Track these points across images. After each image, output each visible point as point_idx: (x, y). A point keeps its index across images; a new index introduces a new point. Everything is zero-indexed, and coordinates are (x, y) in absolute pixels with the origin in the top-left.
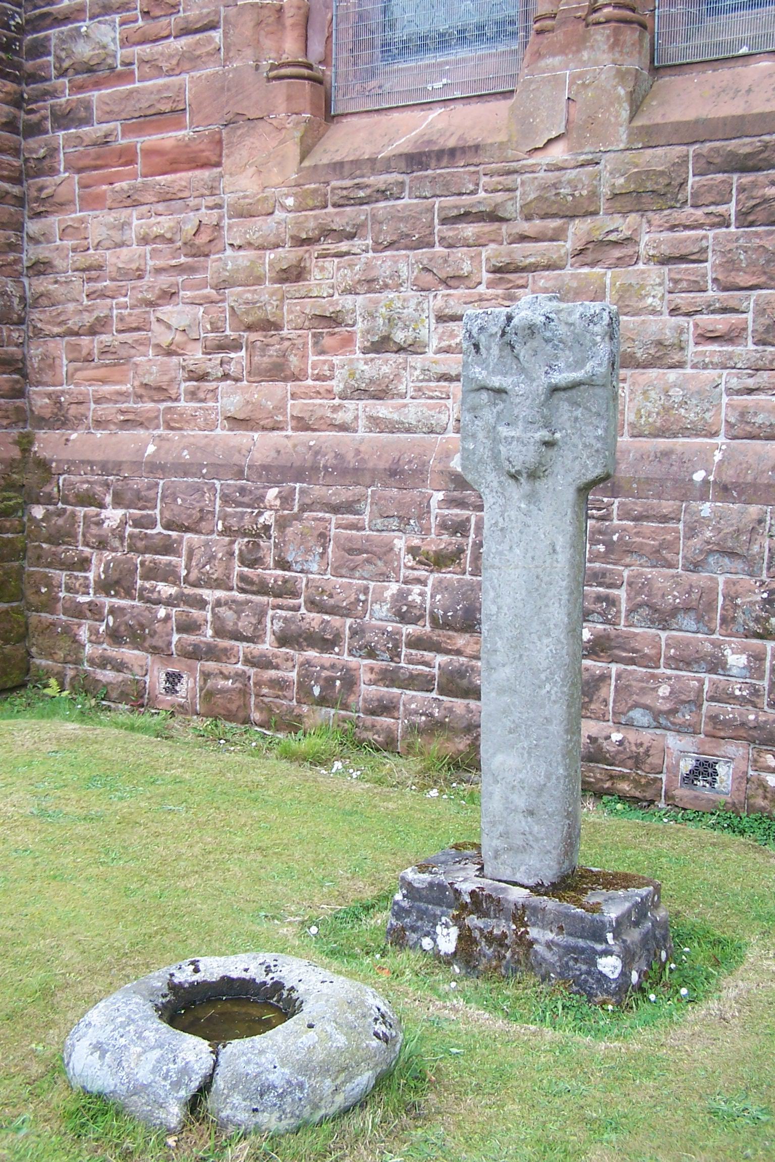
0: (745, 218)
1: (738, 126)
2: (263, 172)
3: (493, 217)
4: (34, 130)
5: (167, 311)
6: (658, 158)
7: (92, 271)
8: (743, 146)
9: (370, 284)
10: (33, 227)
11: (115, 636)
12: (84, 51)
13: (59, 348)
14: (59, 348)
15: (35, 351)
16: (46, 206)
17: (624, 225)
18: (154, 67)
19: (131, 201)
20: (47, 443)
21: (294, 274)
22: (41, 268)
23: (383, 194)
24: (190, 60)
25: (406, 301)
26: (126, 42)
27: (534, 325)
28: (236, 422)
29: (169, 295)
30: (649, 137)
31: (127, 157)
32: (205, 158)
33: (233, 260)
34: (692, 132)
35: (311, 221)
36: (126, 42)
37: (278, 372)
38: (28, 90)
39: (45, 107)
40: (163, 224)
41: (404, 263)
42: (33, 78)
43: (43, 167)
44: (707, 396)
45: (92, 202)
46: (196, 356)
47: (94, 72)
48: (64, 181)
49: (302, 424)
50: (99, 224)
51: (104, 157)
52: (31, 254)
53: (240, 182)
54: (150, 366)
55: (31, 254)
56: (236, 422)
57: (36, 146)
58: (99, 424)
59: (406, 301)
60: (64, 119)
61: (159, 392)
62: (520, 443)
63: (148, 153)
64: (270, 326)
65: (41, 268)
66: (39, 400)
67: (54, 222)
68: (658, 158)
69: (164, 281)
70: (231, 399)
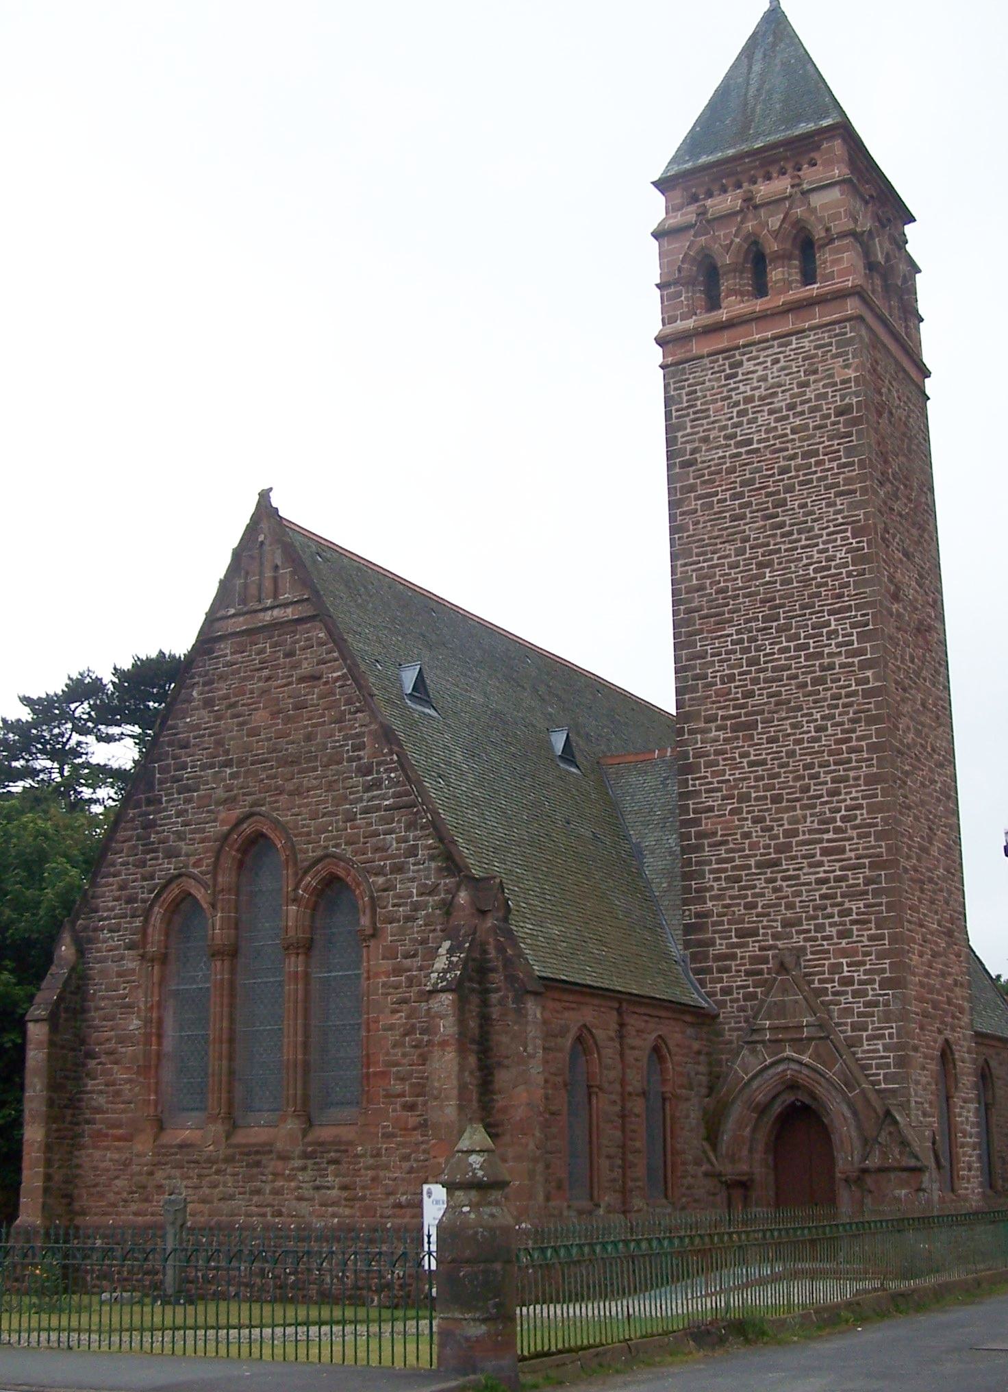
0: (247, 1166)
1: (246, 1145)
2: (143, 1145)
3: (197, 1162)
4: (77, 1124)
5: (116, 1181)
6: (231, 1151)
7: (95, 1168)
8: (246, 1150)
9: (169, 1177)
10: (76, 1153)
11: (98, 1278)
12: (94, 1104)
13: (84, 1191)
14: (84, 1191)
15: (76, 1191)
16: (82, 1147)
17: (224, 1167)
18: (114, 1111)
19: (107, 1148)
20: (79, 1220)
21: (151, 1173)
22: (79, 1166)
23: (172, 1154)
24: (123, 1111)
25: (178, 1182)
26: (107, 1102)
27: (938, 1302)
28: (135, 1214)
29: (117, 1177)
30: (229, 1146)
31: (106, 1135)
32: (128, 1138)
33: (135, 1168)
34: (238, 1146)
35: (157, 1159)
36: (107, 1102)
37: (147, 1200)
38: (77, 1112)
39: (81, 1118)
40: (116, 1156)
41: (177, 1172)
42: (78, 1108)
43: (81, 1135)
44: (239, 1207)
45: (96, 1147)
46: (125, 1195)
47: (98, 1110)
48: (86, 1140)
49: (152, 1215)
50: (97, 1154)
51: (100, 1135)
52: (76, 1161)
53: (138, 1147)
54: (111, 1197)
55: (76, 1161)
56: (135, 1214)
57: (78, 1129)
58: (96, 1214)
59: (178, 1182)
60: (88, 1122)
61: (114, 1205)
62: (171, 1218)
63: (113, 1135)
64: (144, 1187)
65: (79, 1166)
66: (76, 1206)
67: (83, 1152)
68: (231, 1151)
69: (116, 1173)
70: (134, 1207)
